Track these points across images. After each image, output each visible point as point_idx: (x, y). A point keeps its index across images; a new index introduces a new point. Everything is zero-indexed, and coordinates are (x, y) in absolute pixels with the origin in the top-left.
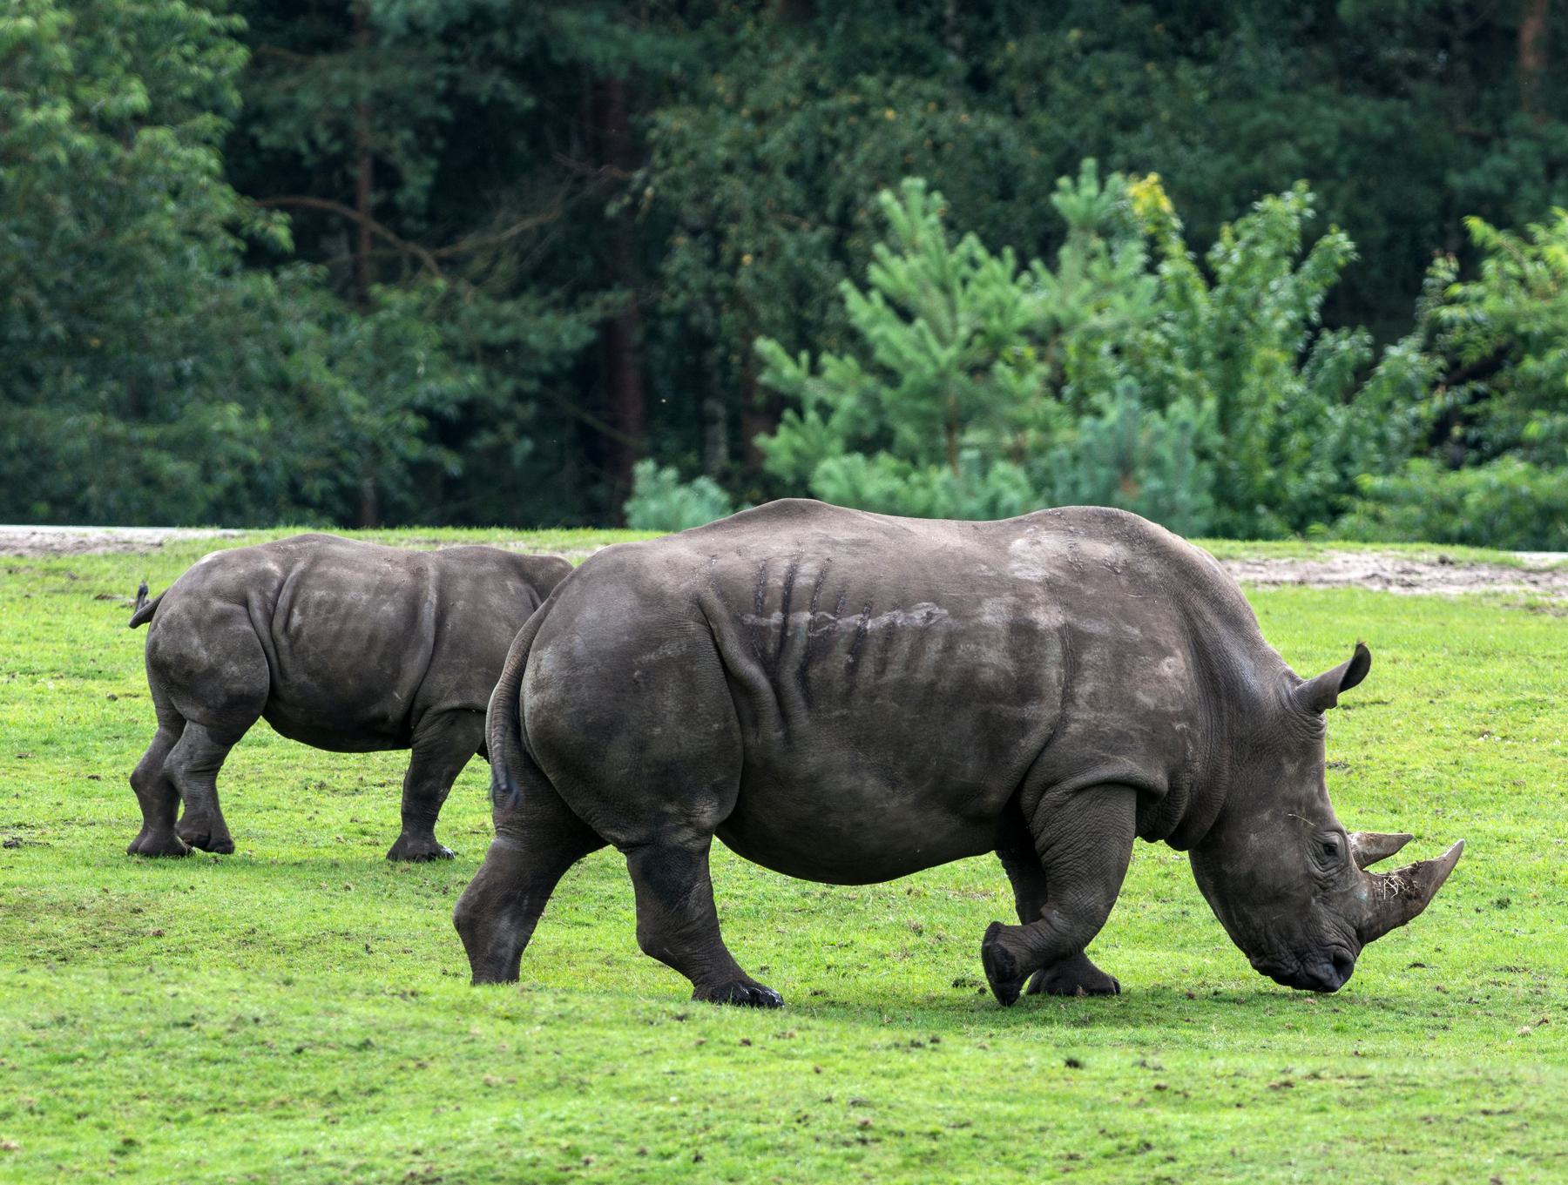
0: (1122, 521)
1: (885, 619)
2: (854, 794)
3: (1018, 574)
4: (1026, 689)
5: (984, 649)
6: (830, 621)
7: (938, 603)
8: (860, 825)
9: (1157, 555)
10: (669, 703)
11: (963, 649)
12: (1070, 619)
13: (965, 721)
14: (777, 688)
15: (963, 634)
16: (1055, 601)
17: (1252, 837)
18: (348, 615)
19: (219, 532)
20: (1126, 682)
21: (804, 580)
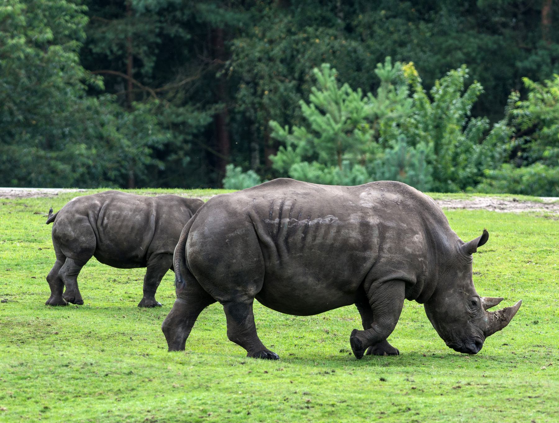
0: (400, 186)
1: (315, 221)
2: (304, 283)
3: (363, 205)
4: (366, 246)
5: (351, 231)
6: (296, 222)
7: (334, 215)
8: (307, 294)
9: (413, 198)
10: (239, 251)
11: (343, 232)
12: (381, 221)
13: (344, 258)
14: (277, 245)
15: (343, 226)
16: (376, 215)
17: (447, 299)
18: (124, 220)
19: (78, 190)
20: (401, 243)
21: (287, 207)
